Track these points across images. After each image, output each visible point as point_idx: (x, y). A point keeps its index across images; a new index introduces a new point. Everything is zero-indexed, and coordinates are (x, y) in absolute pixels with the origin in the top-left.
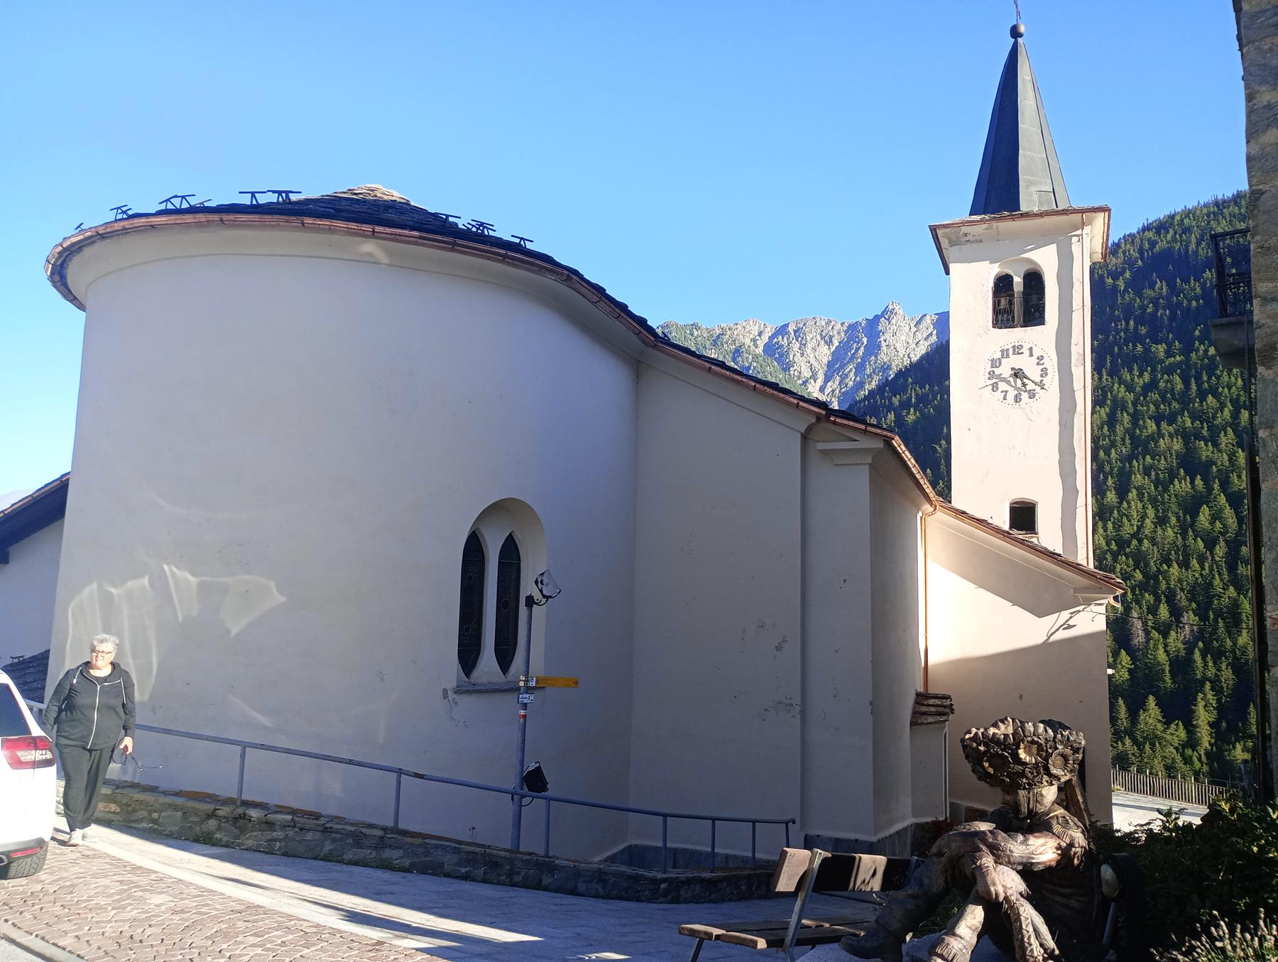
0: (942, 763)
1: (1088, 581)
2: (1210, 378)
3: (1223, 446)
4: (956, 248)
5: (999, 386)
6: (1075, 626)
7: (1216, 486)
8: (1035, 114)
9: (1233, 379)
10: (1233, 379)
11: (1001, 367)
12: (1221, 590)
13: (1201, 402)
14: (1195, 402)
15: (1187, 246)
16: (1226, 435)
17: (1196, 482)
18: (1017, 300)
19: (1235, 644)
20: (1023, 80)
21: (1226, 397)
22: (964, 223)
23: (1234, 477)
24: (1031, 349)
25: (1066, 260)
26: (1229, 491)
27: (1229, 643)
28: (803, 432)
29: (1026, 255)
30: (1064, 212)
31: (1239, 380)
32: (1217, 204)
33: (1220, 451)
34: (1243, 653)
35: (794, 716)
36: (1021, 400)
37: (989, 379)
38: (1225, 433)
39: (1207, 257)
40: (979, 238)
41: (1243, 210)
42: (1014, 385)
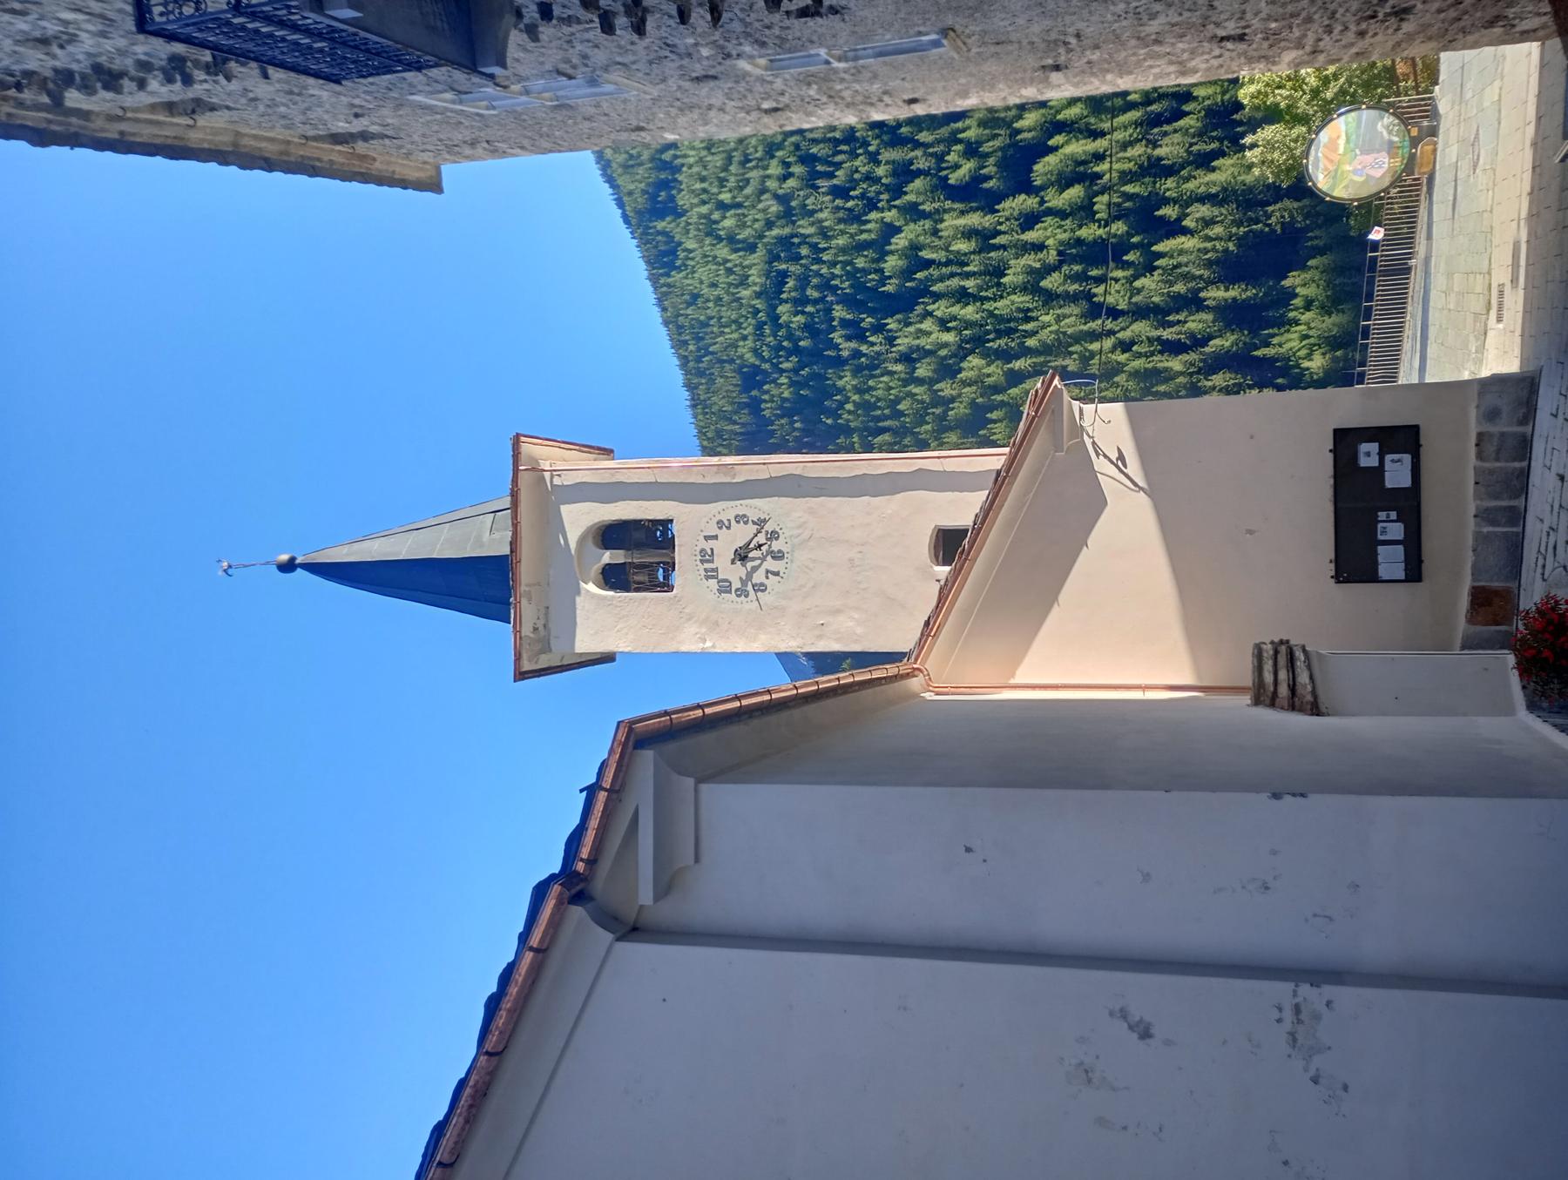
0: (1393, 659)
1: (1043, 428)
2: (879, 408)
3: (954, 393)
4: (553, 642)
5: (758, 582)
6: (1118, 448)
7: (999, 398)
8: (392, 539)
9: (880, 385)
10: (880, 385)
11: (731, 579)
12: (1119, 390)
13: (905, 415)
14: (904, 421)
15: (737, 434)
16: (942, 390)
17: (994, 417)
18: (638, 558)
19: (1182, 373)
20: (347, 555)
21: (900, 391)
22: (517, 631)
23: (989, 381)
24: (707, 538)
25: (582, 492)
26: (1005, 385)
27: (1181, 380)
28: (609, 937)
29: (573, 545)
30: (514, 495)
31: (882, 379)
32: (694, 406)
33: (960, 395)
34: (1192, 364)
35: (1328, 1004)
36: (780, 551)
37: (746, 596)
38: (940, 390)
39: (750, 414)
40: (543, 611)
41: (703, 381)
42: (759, 561)
